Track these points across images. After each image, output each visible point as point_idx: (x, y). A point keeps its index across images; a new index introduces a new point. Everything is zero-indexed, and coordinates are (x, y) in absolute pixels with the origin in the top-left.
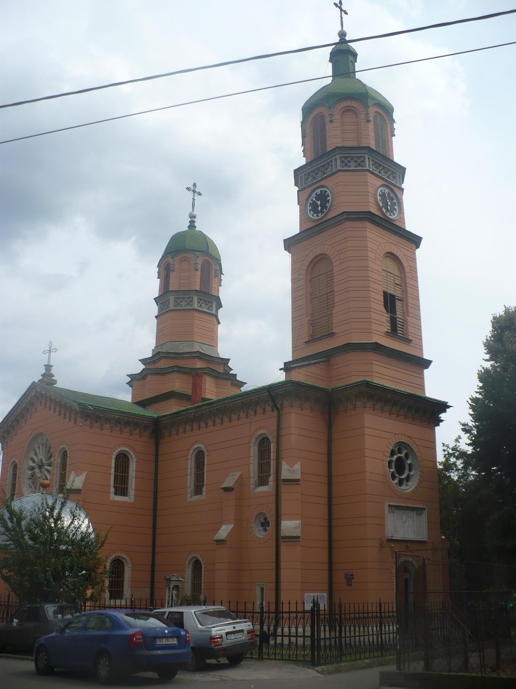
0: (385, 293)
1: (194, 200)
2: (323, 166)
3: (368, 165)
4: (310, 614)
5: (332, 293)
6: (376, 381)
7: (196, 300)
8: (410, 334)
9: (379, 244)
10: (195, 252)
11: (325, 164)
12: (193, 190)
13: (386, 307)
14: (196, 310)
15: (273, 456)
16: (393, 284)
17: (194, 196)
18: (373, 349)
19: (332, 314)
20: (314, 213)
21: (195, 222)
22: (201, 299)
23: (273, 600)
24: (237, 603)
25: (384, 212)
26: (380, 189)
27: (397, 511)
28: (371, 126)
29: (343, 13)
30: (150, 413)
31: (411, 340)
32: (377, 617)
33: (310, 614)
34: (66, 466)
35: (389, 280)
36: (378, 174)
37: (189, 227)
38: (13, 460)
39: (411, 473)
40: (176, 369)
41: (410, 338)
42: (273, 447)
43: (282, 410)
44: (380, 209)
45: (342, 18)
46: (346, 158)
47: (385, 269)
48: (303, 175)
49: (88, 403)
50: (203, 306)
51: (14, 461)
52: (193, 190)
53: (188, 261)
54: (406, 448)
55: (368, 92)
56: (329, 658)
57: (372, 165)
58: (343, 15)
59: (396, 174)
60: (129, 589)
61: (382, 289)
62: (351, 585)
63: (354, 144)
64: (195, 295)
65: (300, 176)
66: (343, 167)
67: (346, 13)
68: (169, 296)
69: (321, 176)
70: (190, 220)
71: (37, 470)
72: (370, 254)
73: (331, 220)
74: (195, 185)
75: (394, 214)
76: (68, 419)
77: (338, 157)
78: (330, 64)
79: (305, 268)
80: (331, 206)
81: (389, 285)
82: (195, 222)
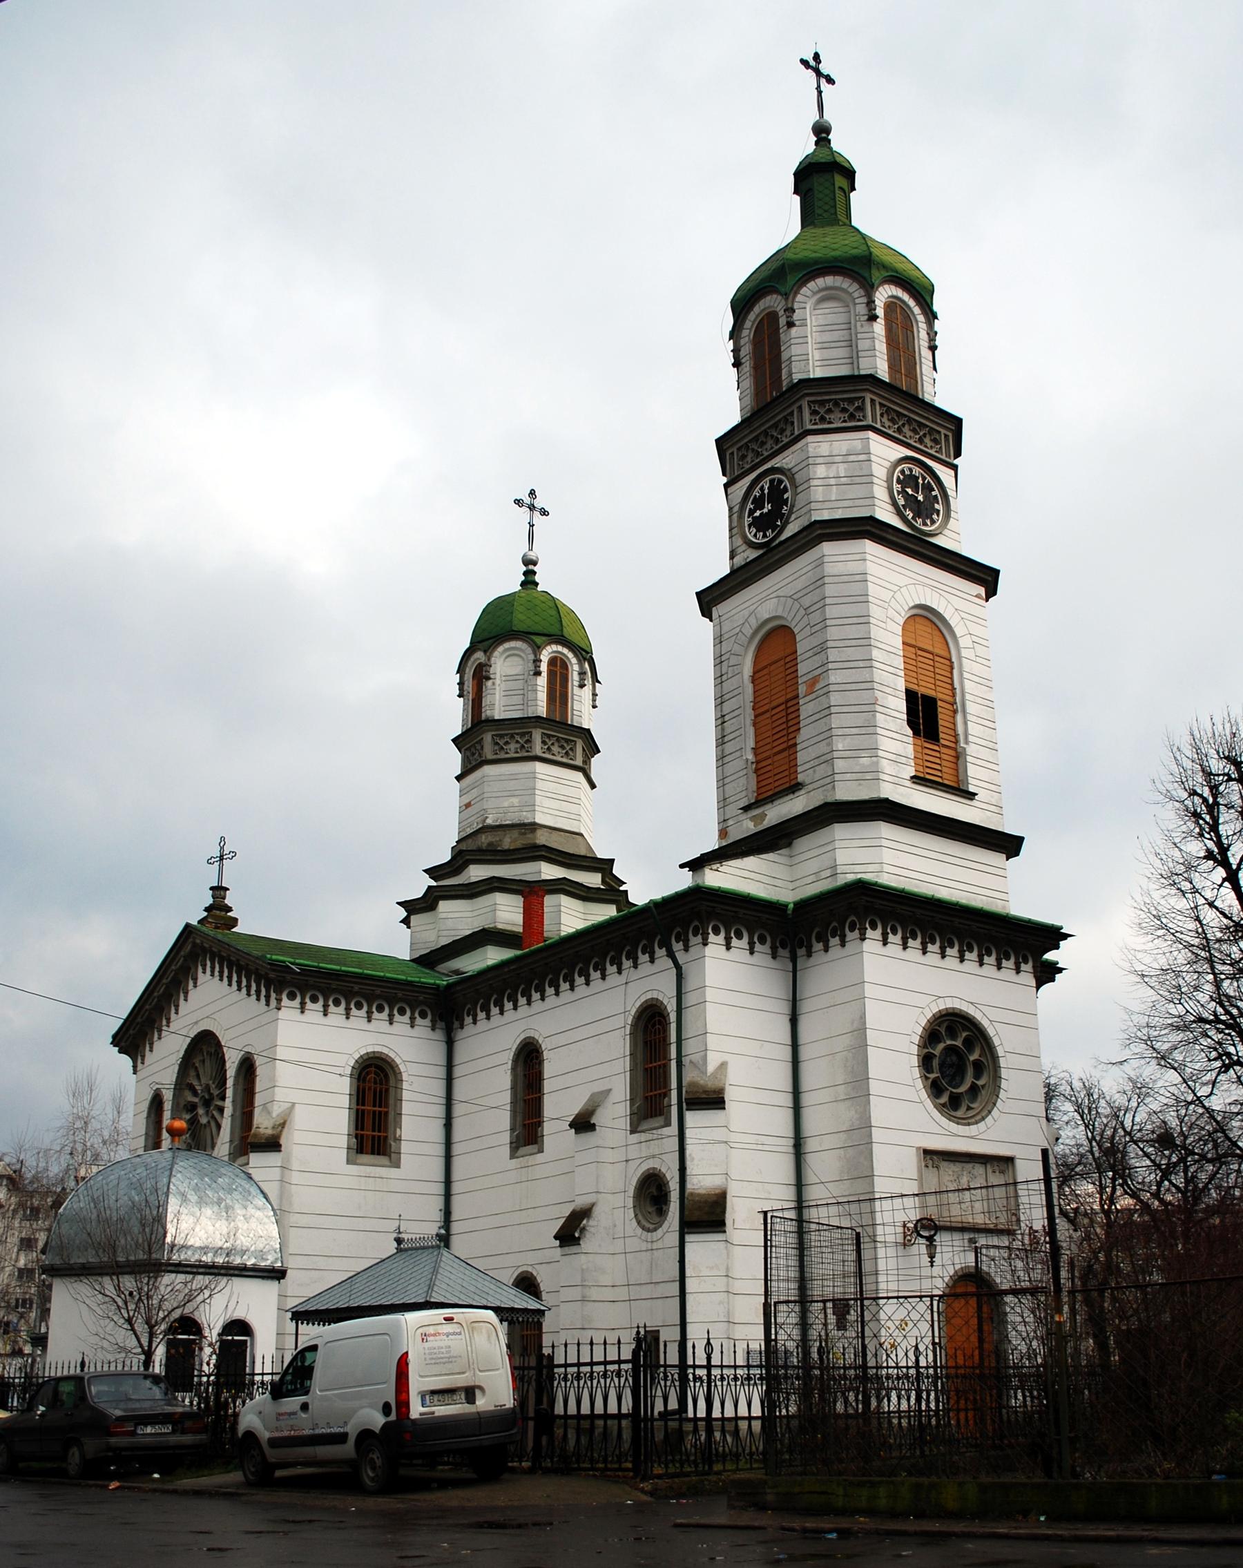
7: (537, 736)
9: (896, 588)
10: (534, 637)
12: (530, 504)
13: (911, 723)
17: (531, 518)
19: (795, 745)
20: (758, 531)
21: (535, 573)
26: (900, 468)
29: (823, 81)
30: (438, 978)
32: (907, 1376)
35: (920, 665)
36: (896, 435)
37: (523, 584)
39: (980, 1083)
41: (972, 789)
45: (820, 93)
46: (822, 403)
48: (735, 449)
50: (555, 749)
52: (530, 504)
54: (965, 1028)
55: (871, 253)
57: (882, 415)
58: (824, 85)
59: (939, 432)
63: (843, 371)
64: (535, 727)
66: (815, 424)
67: (830, 81)
70: (525, 569)
71: (201, 1111)
74: (532, 493)
75: (933, 522)
78: (797, 199)
82: (535, 573)
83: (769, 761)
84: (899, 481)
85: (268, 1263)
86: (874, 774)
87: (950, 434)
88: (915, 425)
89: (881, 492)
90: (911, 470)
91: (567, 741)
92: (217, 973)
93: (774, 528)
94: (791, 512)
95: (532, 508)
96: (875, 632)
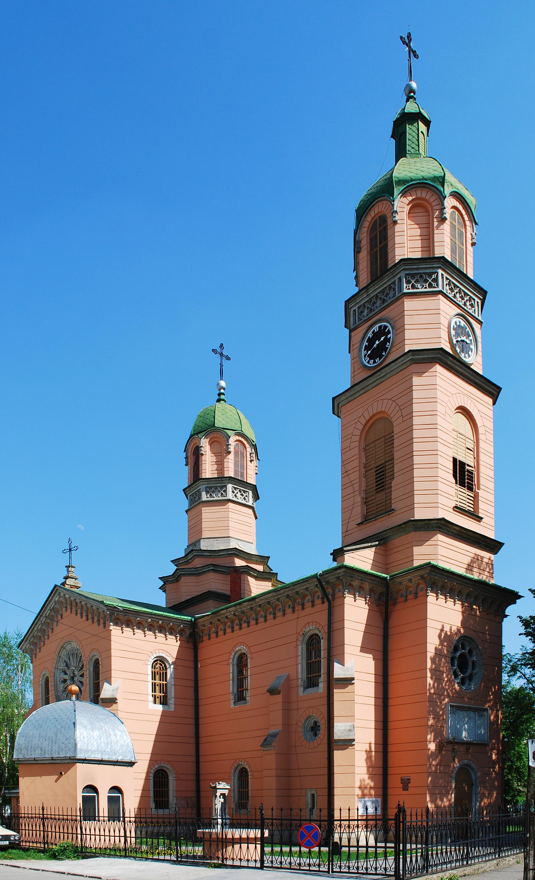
0: (455, 460)
1: (221, 366)
2: (383, 291)
3: (442, 285)
4: (394, 822)
5: (391, 462)
6: (442, 564)
8: (480, 510)
11: (386, 288)
13: (455, 476)
14: (230, 501)
15: (324, 654)
16: (464, 449)
18: (439, 527)
19: (391, 487)
20: (370, 359)
22: (235, 489)
23: (326, 806)
24: (349, 810)
25: (458, 351)
27: (458, 711)
28: (446, 226)
31: (482, 518)
33: (394, 822)
34: (99, 674)
38: (44, 672)
39: (475, 672)
40: (211, 568)
41: (480, 515)
42: (323, 644)
43: (334, 599)
44: (453, 346)
47: (456, 429)
48: (356, 308)
49: (117, 604)
51: (45, 674)
53: (218, 442)
56: (415, 871)
59: (474, 300)
60: (175, 798)
61: (452, 454)
62: (407, 790)
65: (353, 309)
68: (200, 485)
69: (380, 306)
72: (439, 408)
73: (393, 364)
74: (222, 346)
76: (97, 623)
77: (402, 274)
78: (393, 141)
79: (361, 427)
80: (392, 346)
81: (459, 450)
83: (373, 498)
84: (454, 329)
85: (128, 758)
86: (435, 505)
87: (480, 301)
88: (463, 294)
89: (444, 335)
90: (460, 322)
91: (244, 492)
92: (73, 611)
93: (381, 356)
94: (392, 346)
95: (221, 355)
96: (440, 421)
